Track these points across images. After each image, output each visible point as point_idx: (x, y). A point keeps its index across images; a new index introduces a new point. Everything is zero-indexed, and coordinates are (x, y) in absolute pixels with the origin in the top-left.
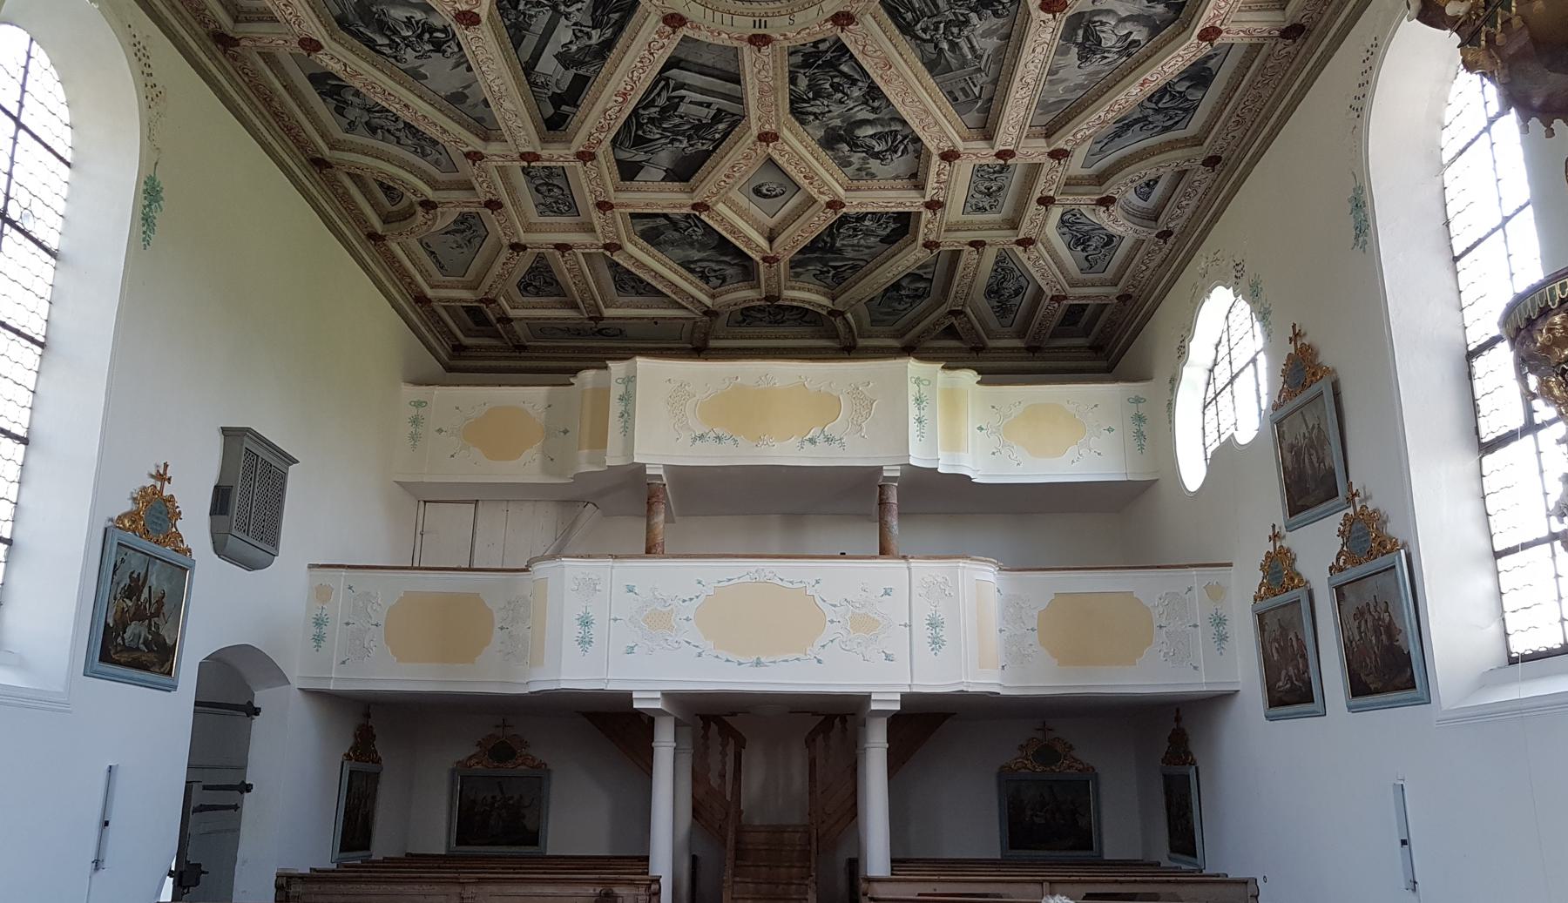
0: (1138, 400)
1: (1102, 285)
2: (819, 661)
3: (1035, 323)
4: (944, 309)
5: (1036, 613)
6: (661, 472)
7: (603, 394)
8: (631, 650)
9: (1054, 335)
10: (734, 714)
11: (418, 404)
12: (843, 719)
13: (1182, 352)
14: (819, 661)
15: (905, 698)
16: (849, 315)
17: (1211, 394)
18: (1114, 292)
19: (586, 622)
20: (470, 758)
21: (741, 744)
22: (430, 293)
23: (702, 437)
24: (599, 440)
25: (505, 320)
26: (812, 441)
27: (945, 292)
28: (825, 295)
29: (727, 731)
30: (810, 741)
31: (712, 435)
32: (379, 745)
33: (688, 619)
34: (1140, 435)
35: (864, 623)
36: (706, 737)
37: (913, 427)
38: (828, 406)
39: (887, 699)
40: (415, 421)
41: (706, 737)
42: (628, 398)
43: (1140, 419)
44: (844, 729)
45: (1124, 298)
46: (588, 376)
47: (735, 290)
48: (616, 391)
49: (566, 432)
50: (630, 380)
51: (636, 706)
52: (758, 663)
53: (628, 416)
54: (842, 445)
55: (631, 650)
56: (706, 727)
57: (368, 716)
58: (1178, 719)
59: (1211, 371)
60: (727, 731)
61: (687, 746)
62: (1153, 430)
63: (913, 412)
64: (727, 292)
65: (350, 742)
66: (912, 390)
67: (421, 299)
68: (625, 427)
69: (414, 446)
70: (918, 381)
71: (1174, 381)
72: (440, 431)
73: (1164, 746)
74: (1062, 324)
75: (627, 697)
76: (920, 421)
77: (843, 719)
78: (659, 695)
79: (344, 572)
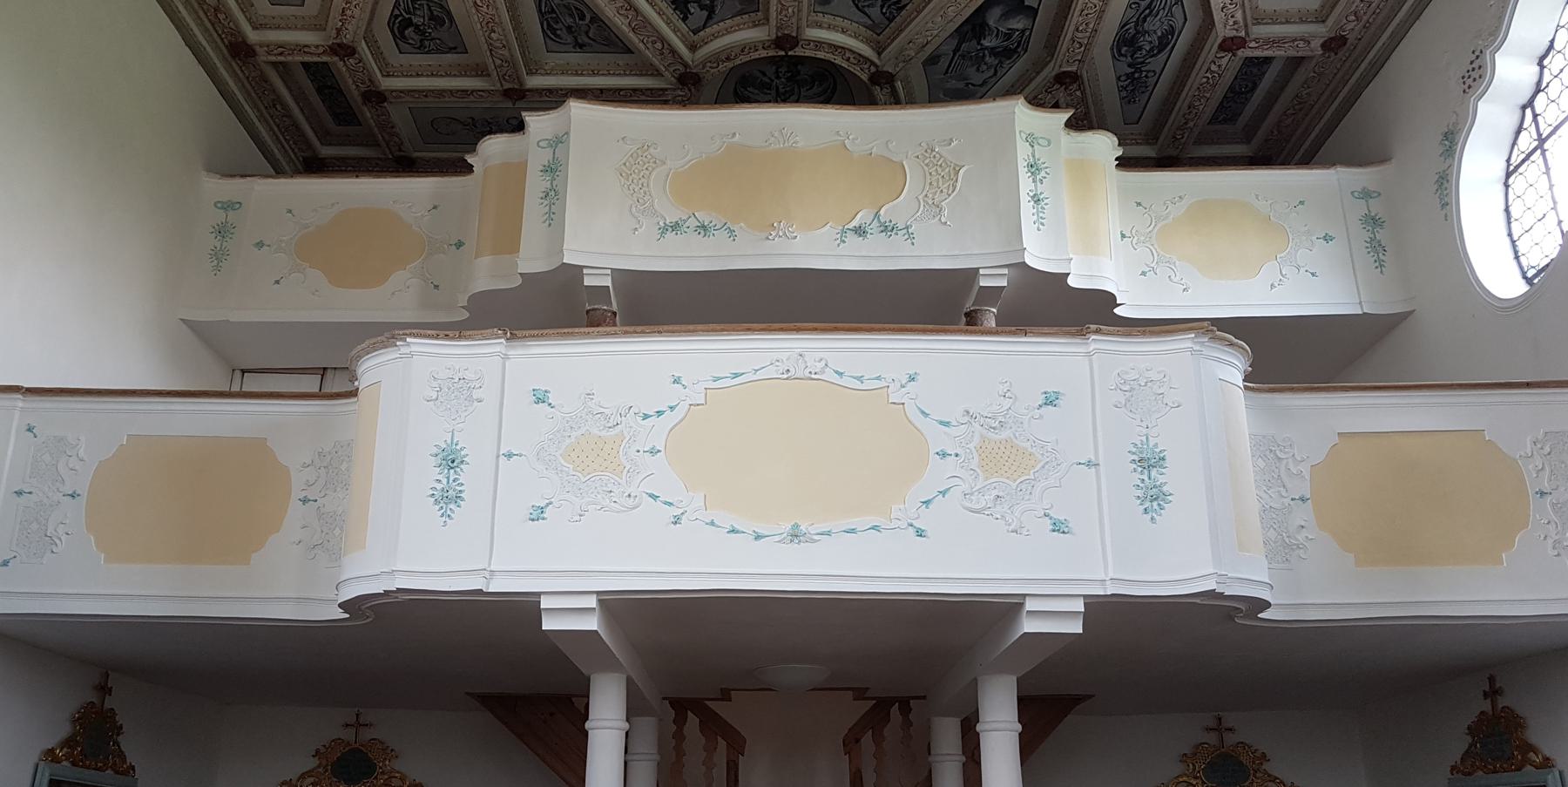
0: (1366, 194)
1: (1302, 21)
2: (920, 533)
3: (1182, 104)
4: (1049, 72)
5: (1305, 470)
6: (608, 282)
7: (515, 172)
8: (538, 514)
9: (1200, 141)
10: (725, 695)
11: (228, 206)
12: (905, 704)
13: (1476, 75)
14: (920, 533)
15: (1100, 610)
16: (899, 84)
17: (1526, 141)
18: (1321, 31)
19: (451, 461)
20: (303, 776)
21: (737, 745)
22: (253, 36)
23: (675, 227)
24: (509, 241)
25: (376, 97)
26: (860, 231)
27: (1051, 45)
28: (867, 41)
29: (714, 726)
30: (851, 743)
31: (693, 223)
32: (132, 746)
33: (653, 452)
34: (1376, 247)
35: (1003, 456)
36: (679, 736)
37: (1027, 207)
38: (884, 175)
39: (1054, 615)
40: (222, 231)
41: (679, 736)
42: (553, 169)
43: (1373, 221)
44: (907, 724)
45: (1334, 44)
46: (494, 148)
47: (728, 32)
48: (538, 159)
49: (459, 245)
50: (559, 141)
51: (548, 624)
52: (795, 535)
53: (554, 197)
54: (910, 236)
55: (538, 514)
56: (680, 720)
57: (104, 689)
58: (1493, 693)
59: (1530, 103)
60: (714, 726)
61: (647, 745)
62: (1416, 226)
63: (1026, 185)
64: (715, 37)
65: (64, 731)
66: (1023, 152)
67: (240, 50)
68: (550, 213)
69: (218, 268)
70: (1031, 140)
71: (1451, 141)
72: (260, 245)
73: (1458, 744)
74: (1214, 120)
75: (525, 608)
76: (1036, 199)
77: (905, 704)
78: (592, 602)
79: (19, 401)
